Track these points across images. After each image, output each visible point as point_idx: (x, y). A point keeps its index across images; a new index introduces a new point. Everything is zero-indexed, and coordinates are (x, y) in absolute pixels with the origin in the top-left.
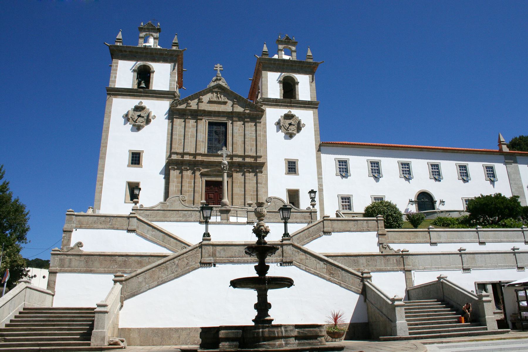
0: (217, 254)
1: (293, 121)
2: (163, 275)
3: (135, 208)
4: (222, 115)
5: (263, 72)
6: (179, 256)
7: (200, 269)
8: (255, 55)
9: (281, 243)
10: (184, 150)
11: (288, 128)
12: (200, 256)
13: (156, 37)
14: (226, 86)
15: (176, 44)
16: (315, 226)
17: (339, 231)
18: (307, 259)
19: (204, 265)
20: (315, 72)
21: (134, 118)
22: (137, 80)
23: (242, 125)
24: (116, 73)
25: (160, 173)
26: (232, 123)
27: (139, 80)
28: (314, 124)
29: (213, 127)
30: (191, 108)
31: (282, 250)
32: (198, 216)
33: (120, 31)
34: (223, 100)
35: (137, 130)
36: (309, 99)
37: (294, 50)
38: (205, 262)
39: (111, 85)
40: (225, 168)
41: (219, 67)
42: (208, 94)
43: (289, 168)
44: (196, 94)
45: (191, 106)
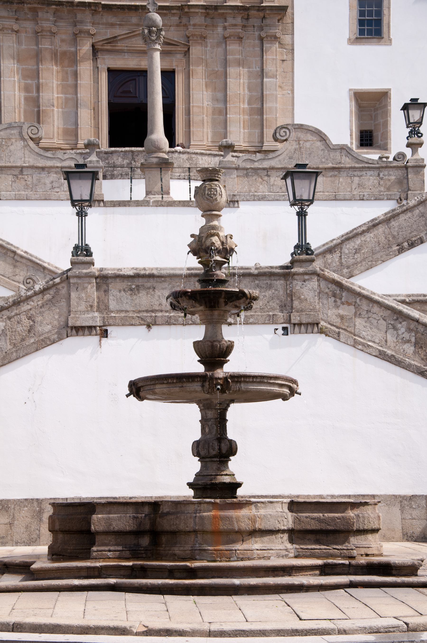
38: (78, 324)
43: (361, 23)
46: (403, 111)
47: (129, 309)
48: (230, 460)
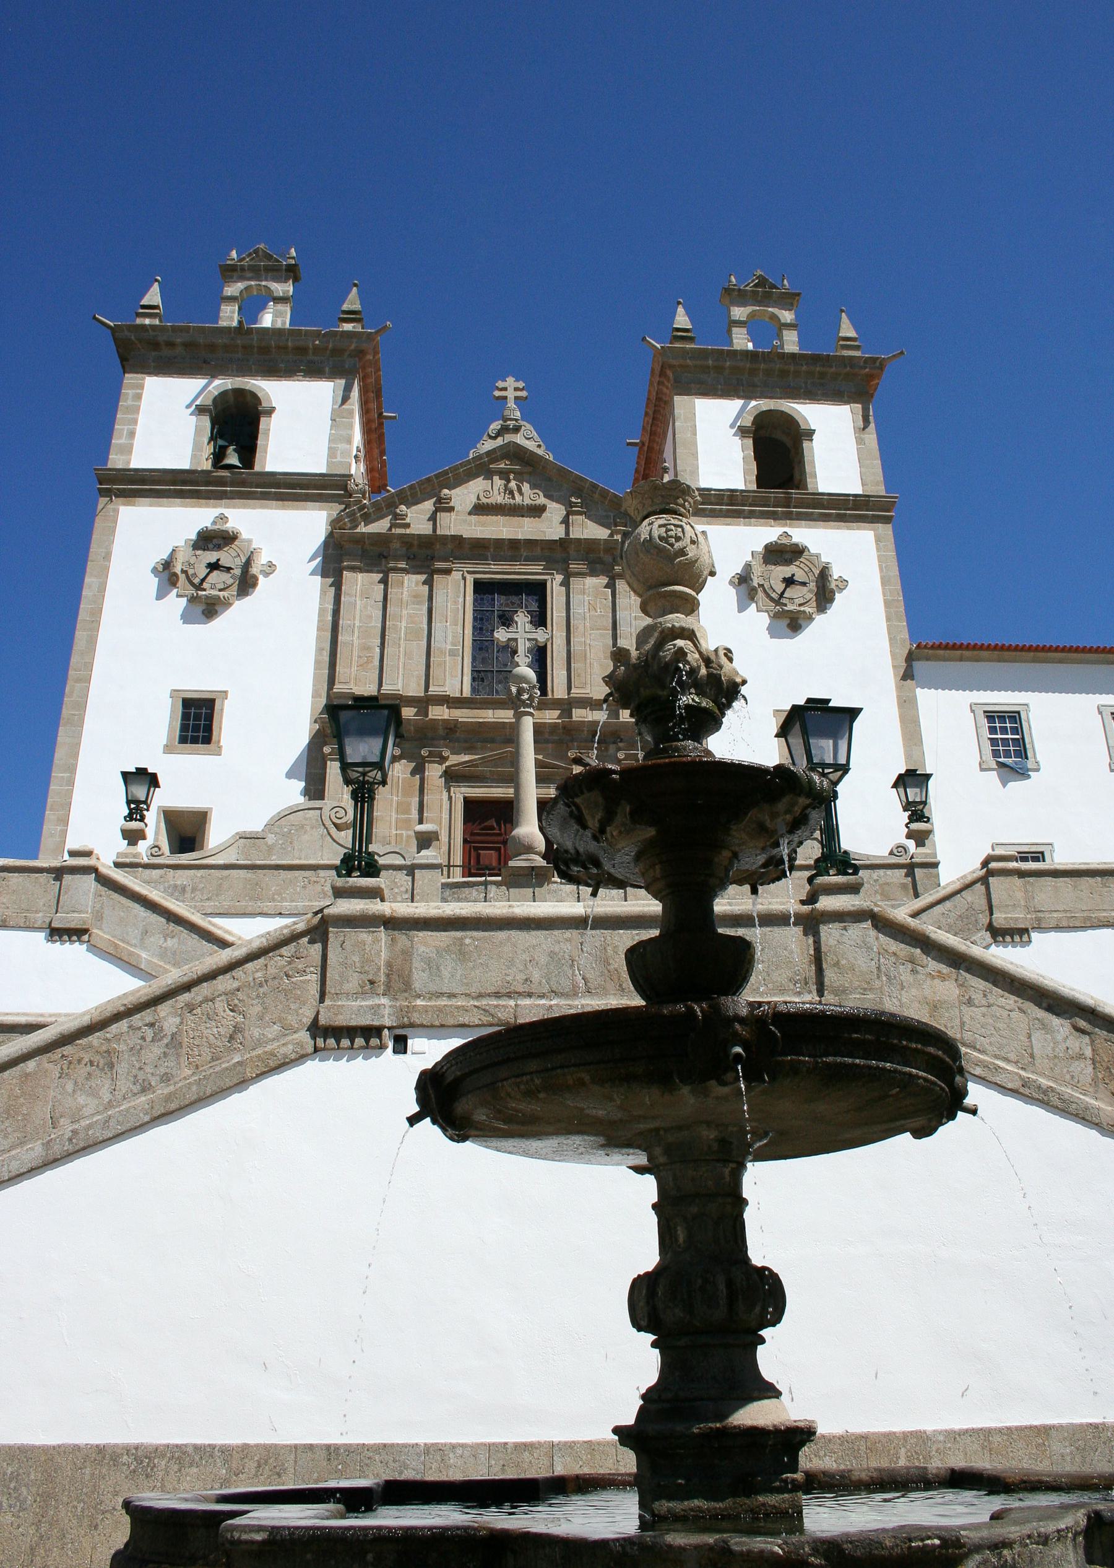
0: (420, 979)
1: (799, 569)
2: (82, 1099)
3: (126, 857)
4: (524, 553)
5: (677, 398)
6: (187, 987)
7: (312, 1066)
8: (644, 339)
9: (806, 908)
10: (380, 684)
11: (781, 595)
12: (314, 990)
13: (281, 295)
14: (540, 452)
15: (352, 316)
16: (948, 904)
17: (1065, 924)
18: (970, 1002)
19: (338, 1042)
20: (872, 396)
21: (195, 575)
22: (209, 443)
23: (605, 587)
24: (135, 422)
25: (290, 775)
26: (566, 584)
27: (220, 442)
28: (882, 578)
29: (493, 599)
30: (408, 531)
31: (812, 952)
32: (403, 889)
33: (156, 280)
34: (527, 501)
35: (203, 617)
36: (854, 488)
37: (789, 321)
38: (341, 1020)
39: (116, 461)
40: (526, 696)
41: (511, 387)
42: (470, 483)
44: (429, 480)
45: (408, 526)
46: (895, 789)
47: (457, 991)
48: (762, 1341)
